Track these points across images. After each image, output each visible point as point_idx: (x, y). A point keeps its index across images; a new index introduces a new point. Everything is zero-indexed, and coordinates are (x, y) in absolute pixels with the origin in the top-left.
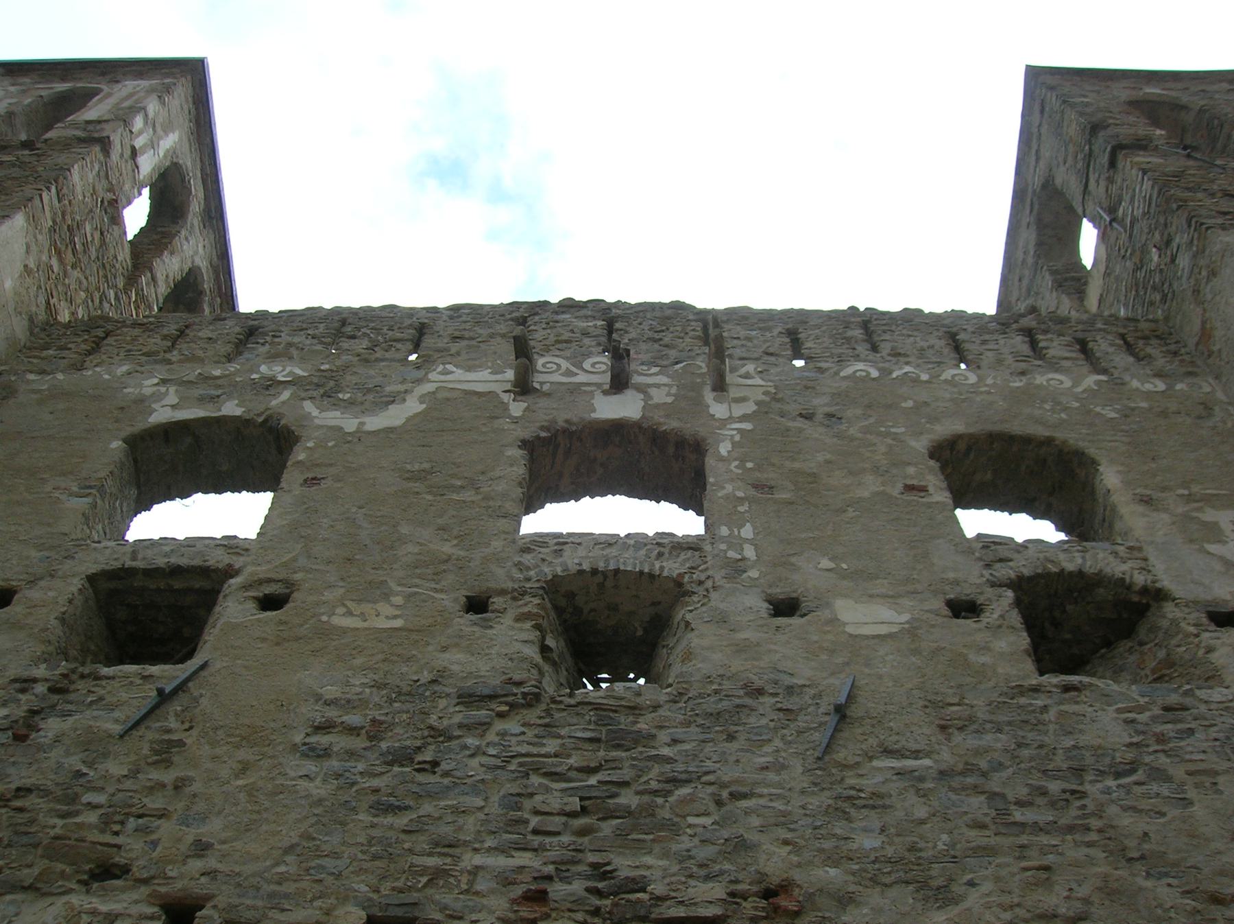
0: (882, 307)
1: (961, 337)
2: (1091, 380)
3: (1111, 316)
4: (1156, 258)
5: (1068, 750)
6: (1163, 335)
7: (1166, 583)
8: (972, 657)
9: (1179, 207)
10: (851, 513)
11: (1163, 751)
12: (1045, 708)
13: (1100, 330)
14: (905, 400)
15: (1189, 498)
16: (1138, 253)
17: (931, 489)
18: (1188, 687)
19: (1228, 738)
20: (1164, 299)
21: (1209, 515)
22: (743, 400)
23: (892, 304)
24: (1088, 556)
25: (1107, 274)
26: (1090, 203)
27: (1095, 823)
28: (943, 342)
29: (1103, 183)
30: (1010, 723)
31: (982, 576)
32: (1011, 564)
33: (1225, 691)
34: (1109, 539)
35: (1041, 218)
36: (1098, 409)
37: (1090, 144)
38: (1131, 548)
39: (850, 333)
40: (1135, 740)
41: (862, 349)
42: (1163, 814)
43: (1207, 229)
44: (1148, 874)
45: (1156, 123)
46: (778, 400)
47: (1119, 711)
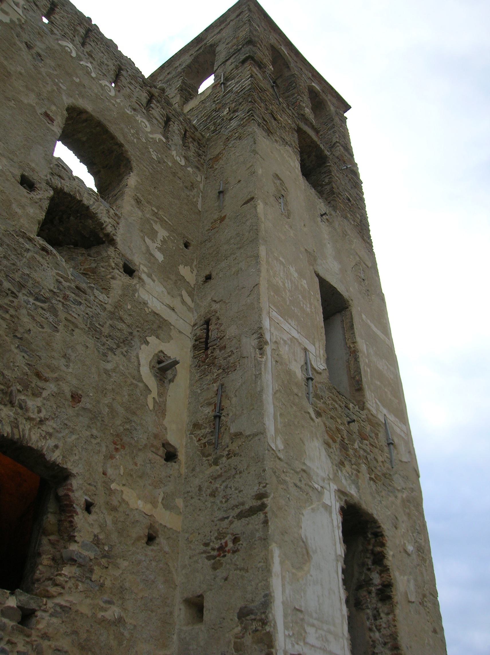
0: (102, 30)
1: (124, 73)
2: (158, 136)
3: (189, 119)
4: (225, 113)
5: (24, 274)
6: (202, 145)
7: (118, 239)
8: (14, 206)
9: (251, 102)
10: (12, 104)
11: (63, 303)
12: (28, 250)
13: (180, 120)
14: (77, 77)
15: (155, 214)
16: (221, 105)
17: (55, 123)
18: (93, 286)
19: (92, 317)
20: (215, 130)
21: (157, 227)
22: (6, 13)
23: (108, 32)
24: (96, 203)
25: (202, 102)
26: (221, 69)
27: (12, 311)
28: (114, 68)
29: (233, 66)
30: (8, 245)
31: (46, 176)
32: (62, 181)
33: (106, 298)
34: (111, 204)
35: (198, 56)
36: (151, 150)
37: (243, 46)
38: (116, 214)
39: (78, 28)
40: (55, 290)
41: (78, 39)
42: (43, 327)
43: (253, 119)
44: (18, 347)
45: (274, 63)
46: (22, 28)
47: (58, 274)
